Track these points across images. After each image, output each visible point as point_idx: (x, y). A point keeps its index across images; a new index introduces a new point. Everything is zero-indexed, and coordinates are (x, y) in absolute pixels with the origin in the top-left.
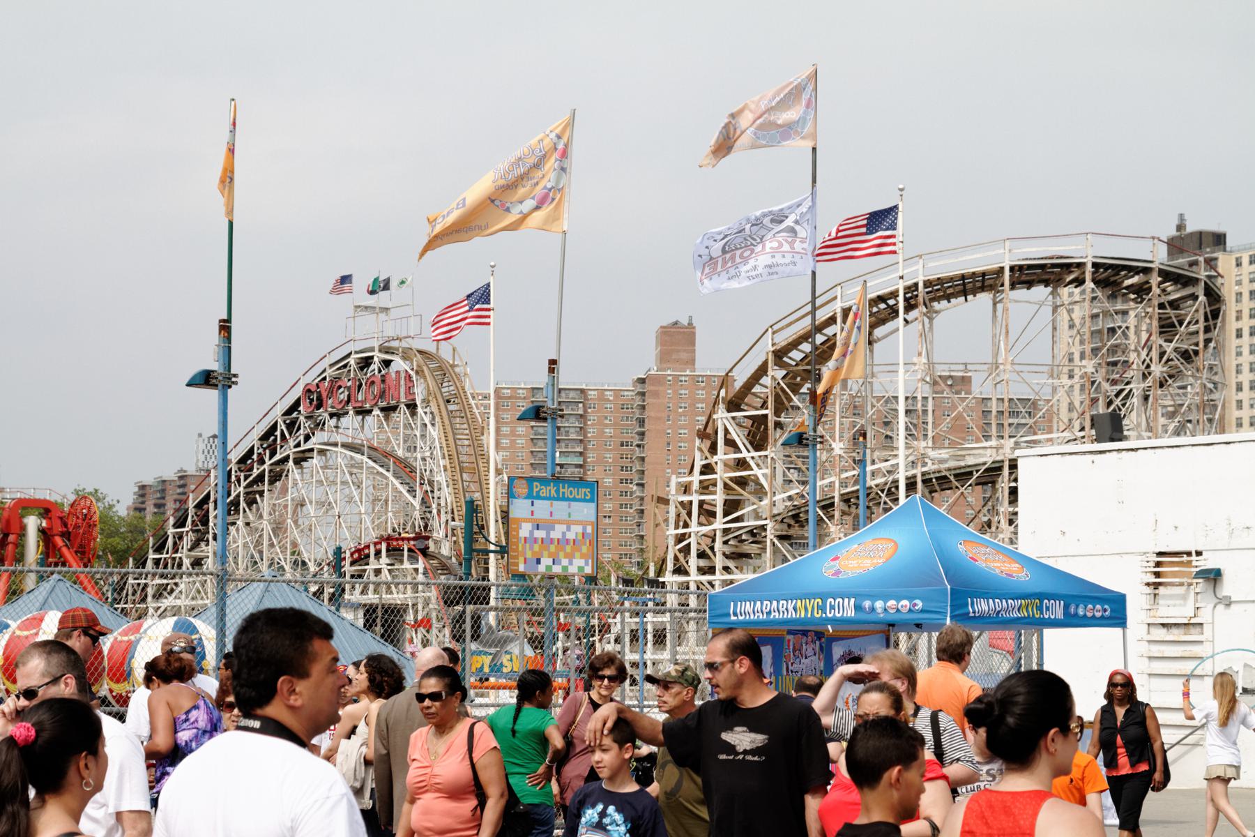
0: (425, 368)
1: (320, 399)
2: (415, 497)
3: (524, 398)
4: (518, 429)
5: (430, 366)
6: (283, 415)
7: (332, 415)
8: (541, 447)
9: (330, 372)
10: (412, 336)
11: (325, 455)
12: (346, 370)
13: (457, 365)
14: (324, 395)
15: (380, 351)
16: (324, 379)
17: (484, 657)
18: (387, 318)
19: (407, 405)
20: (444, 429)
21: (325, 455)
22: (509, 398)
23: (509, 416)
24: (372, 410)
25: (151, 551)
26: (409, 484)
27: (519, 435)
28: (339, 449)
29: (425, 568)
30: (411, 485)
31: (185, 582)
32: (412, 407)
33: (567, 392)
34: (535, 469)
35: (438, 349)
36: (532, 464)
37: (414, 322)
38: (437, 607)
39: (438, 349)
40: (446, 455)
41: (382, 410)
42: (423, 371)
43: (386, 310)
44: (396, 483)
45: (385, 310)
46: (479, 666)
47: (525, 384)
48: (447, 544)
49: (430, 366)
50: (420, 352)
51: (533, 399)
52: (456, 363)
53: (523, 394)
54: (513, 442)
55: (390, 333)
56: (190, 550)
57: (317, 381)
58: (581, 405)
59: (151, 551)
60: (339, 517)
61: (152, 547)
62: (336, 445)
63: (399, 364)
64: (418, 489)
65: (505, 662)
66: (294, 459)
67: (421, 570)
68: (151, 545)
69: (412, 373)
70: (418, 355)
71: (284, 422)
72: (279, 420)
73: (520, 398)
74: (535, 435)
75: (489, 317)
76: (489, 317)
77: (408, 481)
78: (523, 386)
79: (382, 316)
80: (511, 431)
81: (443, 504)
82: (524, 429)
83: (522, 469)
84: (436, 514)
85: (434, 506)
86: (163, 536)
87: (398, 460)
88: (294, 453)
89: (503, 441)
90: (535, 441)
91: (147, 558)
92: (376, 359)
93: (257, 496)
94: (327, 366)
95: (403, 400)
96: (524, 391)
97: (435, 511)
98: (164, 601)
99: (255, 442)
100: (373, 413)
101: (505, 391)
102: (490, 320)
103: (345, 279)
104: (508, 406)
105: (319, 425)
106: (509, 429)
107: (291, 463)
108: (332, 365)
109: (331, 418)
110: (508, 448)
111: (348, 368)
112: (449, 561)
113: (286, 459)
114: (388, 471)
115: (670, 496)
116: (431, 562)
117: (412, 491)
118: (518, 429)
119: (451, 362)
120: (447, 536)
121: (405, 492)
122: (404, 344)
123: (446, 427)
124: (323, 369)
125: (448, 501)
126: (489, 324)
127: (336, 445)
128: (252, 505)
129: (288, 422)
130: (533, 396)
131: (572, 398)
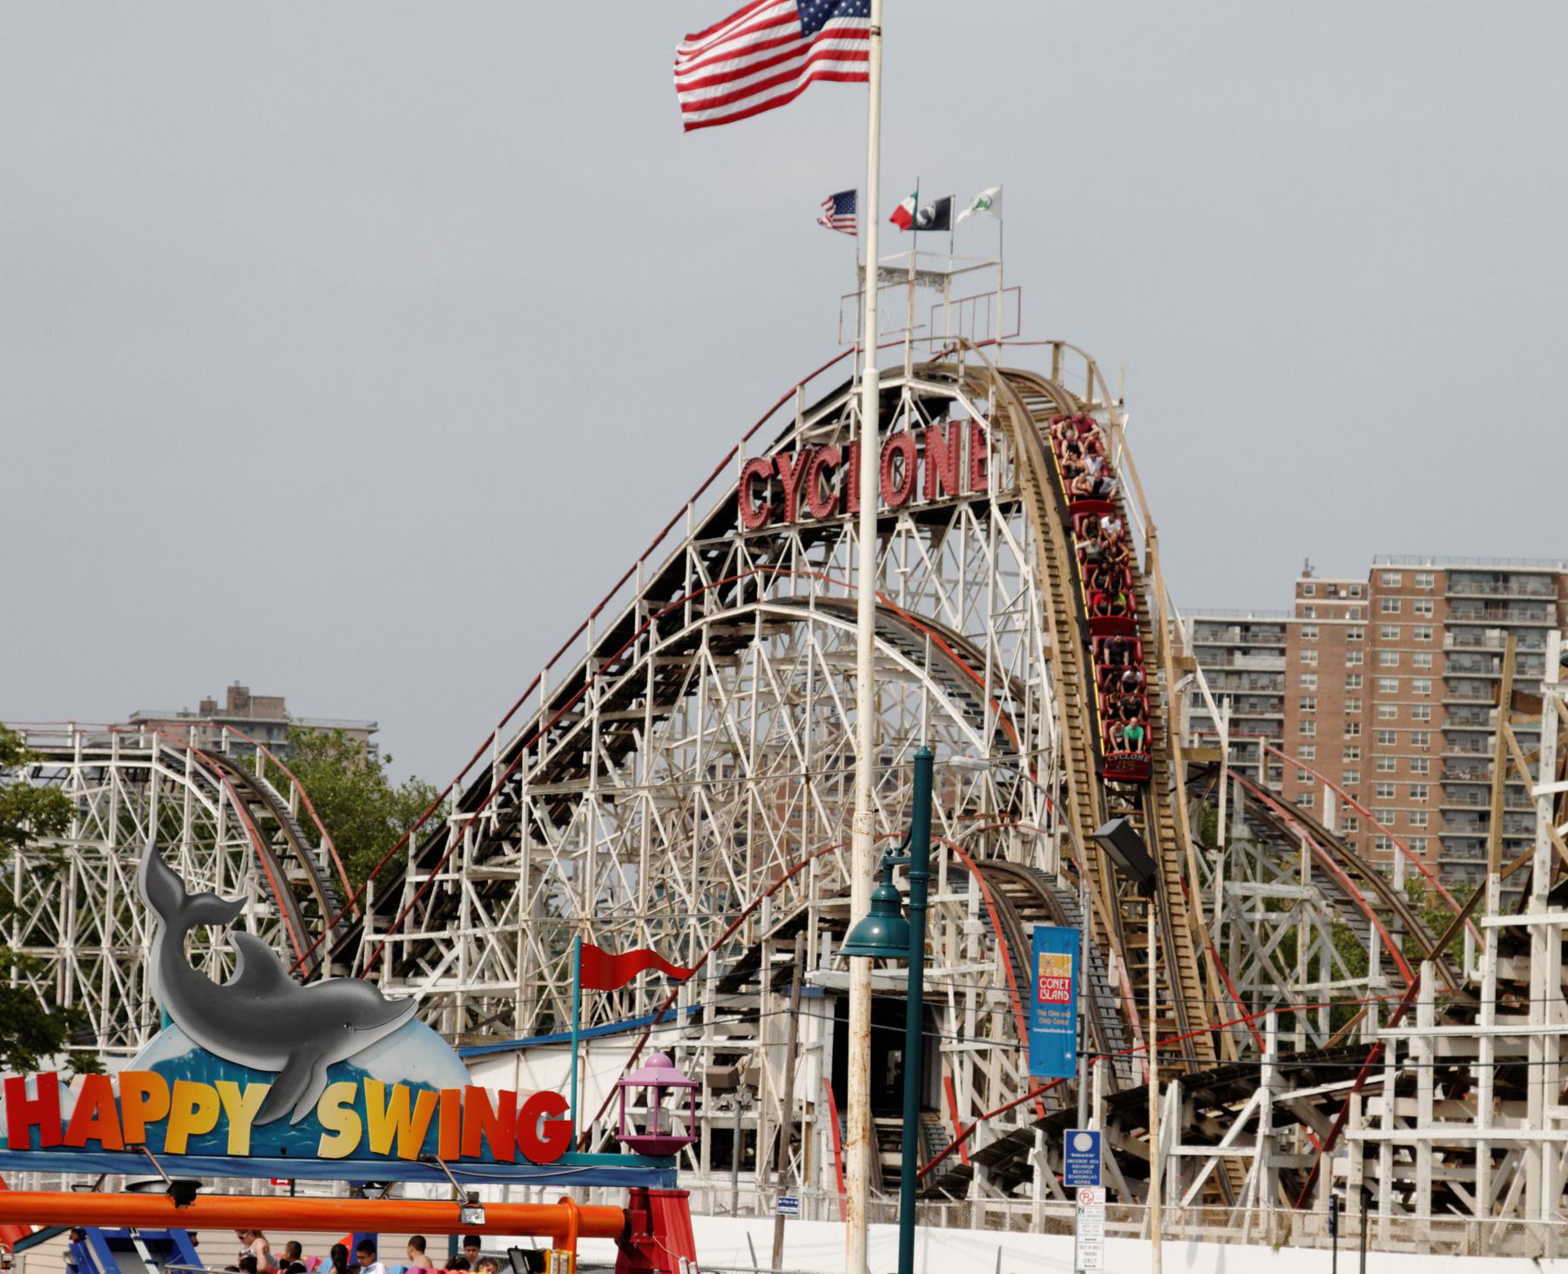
0: (1013, 411)
1: (778, 497)
2: (980, 727)
3: (1432, 592)
4: (1417, 657)
5: (1030, 407)
6: (697, 538)
7: (808, 537)
8: (1466, 697)
9: (803, 428)
10: (998, 339)
11: (789, 631)
12: (835, 425)
13: (1098, 407)
14: (789, 485)
15: (917, 375)
16: (791, 446)
17: (228, 1088)
18: (940, 298)
19: (972, 505)
20: (1051, 558)
21: (789, 631)
22: (1399, 591)
23: (1397, 630)
24: (896, 520)
25: (412, 865)
26: (967, 696)
27: (1420, 671)
28: (812, 614)
29: (982, 903)
30: (975, 699)
31: (466, 936)
32: (981, 509)
33: (1523, 579)
34: (1452, 742)
35: (1055, 369)
36: (1445, 732)
37: (1003, 305)
38: (1005, 999)
39: (1055, 369)
40: (1052, 621)
41: (921, 518)
42: (1007, 418)
43: (939, 279)
44: (938, 692)
45: (939, 279)
46: (205, 1123)
47: (1433, 563)
48: (1048, 842)
49: (1030, 407)
50: (1009, 376)
51: (1451, 595)
52: (1095, 401)
53: (1428, 583)
54: (1406, 685)
55: (948, 326)
56: (479, 860)
57: (773, 452)
58: (1551, 608)
59: (412, 865)
60: (808, 779)
61: (415, 857)
62: (803, 603)
63: (963, 408)
64: (987, 707)
65: (329, 1115)
66: (711, 640)
67: (974, 907)
68: (412, 852)
69: (983, 424)
70: (999, 378)
71: (703, 554)
72: (690, 550)
73: (1421, 592)
74: (1454, 669)
75: (864, 56)
76: (864, 56)
77: (966, 690)
78: (1428, 566)
79: (926, 293)
80: (1403, 662)
81: (1042, 745)
82: (1429, 658)
83: (1424, 742)
84: (1027, 772)
85: (1023, 749)
86: (436, 832)
87: (946, 639)
88: (712, 624)
89: (1383, 682)
90: (1453, 683)
91: (403, 883)
92: (906, 395)
93: (636, 732)
94: (797, 416)
95: (965, 493)
96: (1432, 578)
97: (1024, 763)
98: (420, 980)
99: (636, 603)
100: (899, 526)
101: (1391, 577)
102: (871, 67)
103: (844, 202)
104: (1395, 608)
105: (782, 564)
106: (1397, 657)
107: (704, 650)
108: (807, 414)
109: (807, 546)
110: (1395, 697)
111: (843, 422)
112: (1049, 886)
113: (694, 640)
114: (920, 664)
115: (1543, 689)
116: (1005, 887)
117: (974, 715)
118: (1417, 657)
119: (1084, 400)
120: (1049, 826)
121: (957, 716)
122: (972, 359)
123: (1056, 553)
124: (788, 423)
125: (1054, 737)
126: (864, 77)
127: (803, 603)
128: (624, 753)
129: (713, 554)
130: (1450, 588)
131: (1534, 593)
